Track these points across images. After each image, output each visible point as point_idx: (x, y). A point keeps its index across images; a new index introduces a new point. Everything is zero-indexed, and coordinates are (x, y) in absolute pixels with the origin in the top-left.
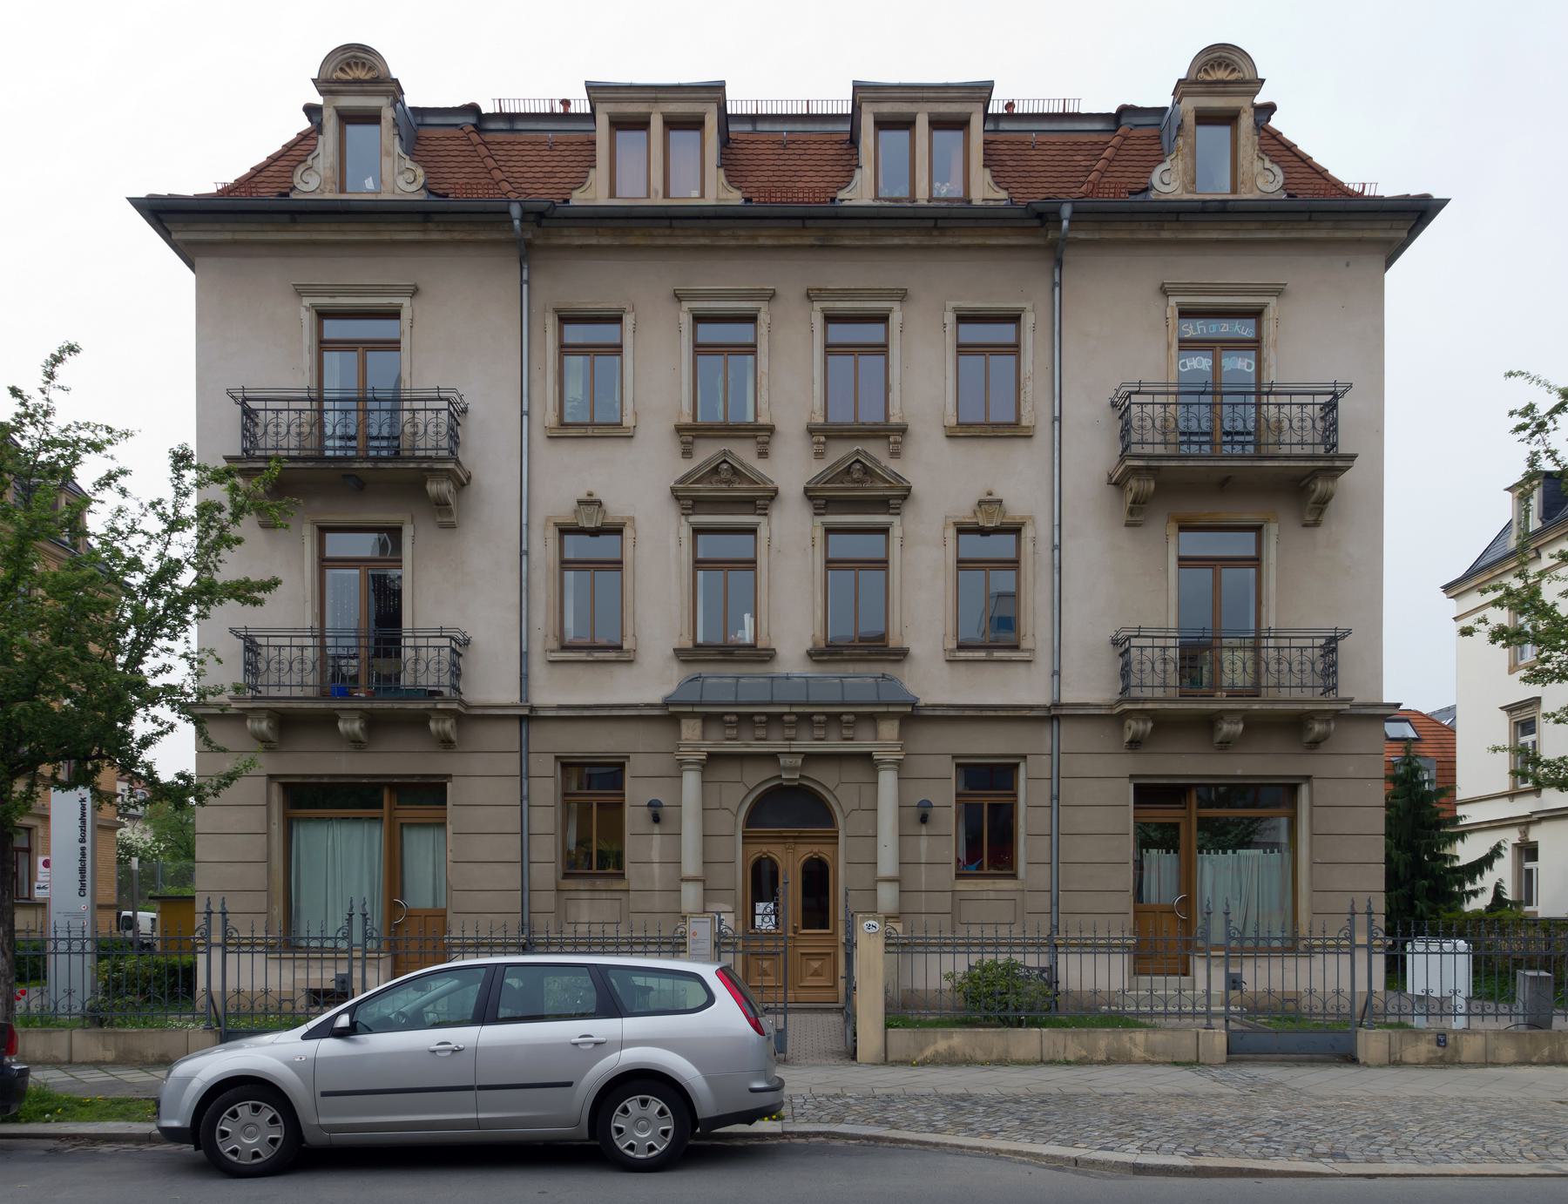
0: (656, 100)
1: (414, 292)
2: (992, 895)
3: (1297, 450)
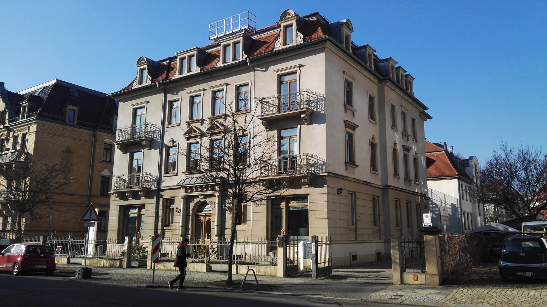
2: (241, 229)
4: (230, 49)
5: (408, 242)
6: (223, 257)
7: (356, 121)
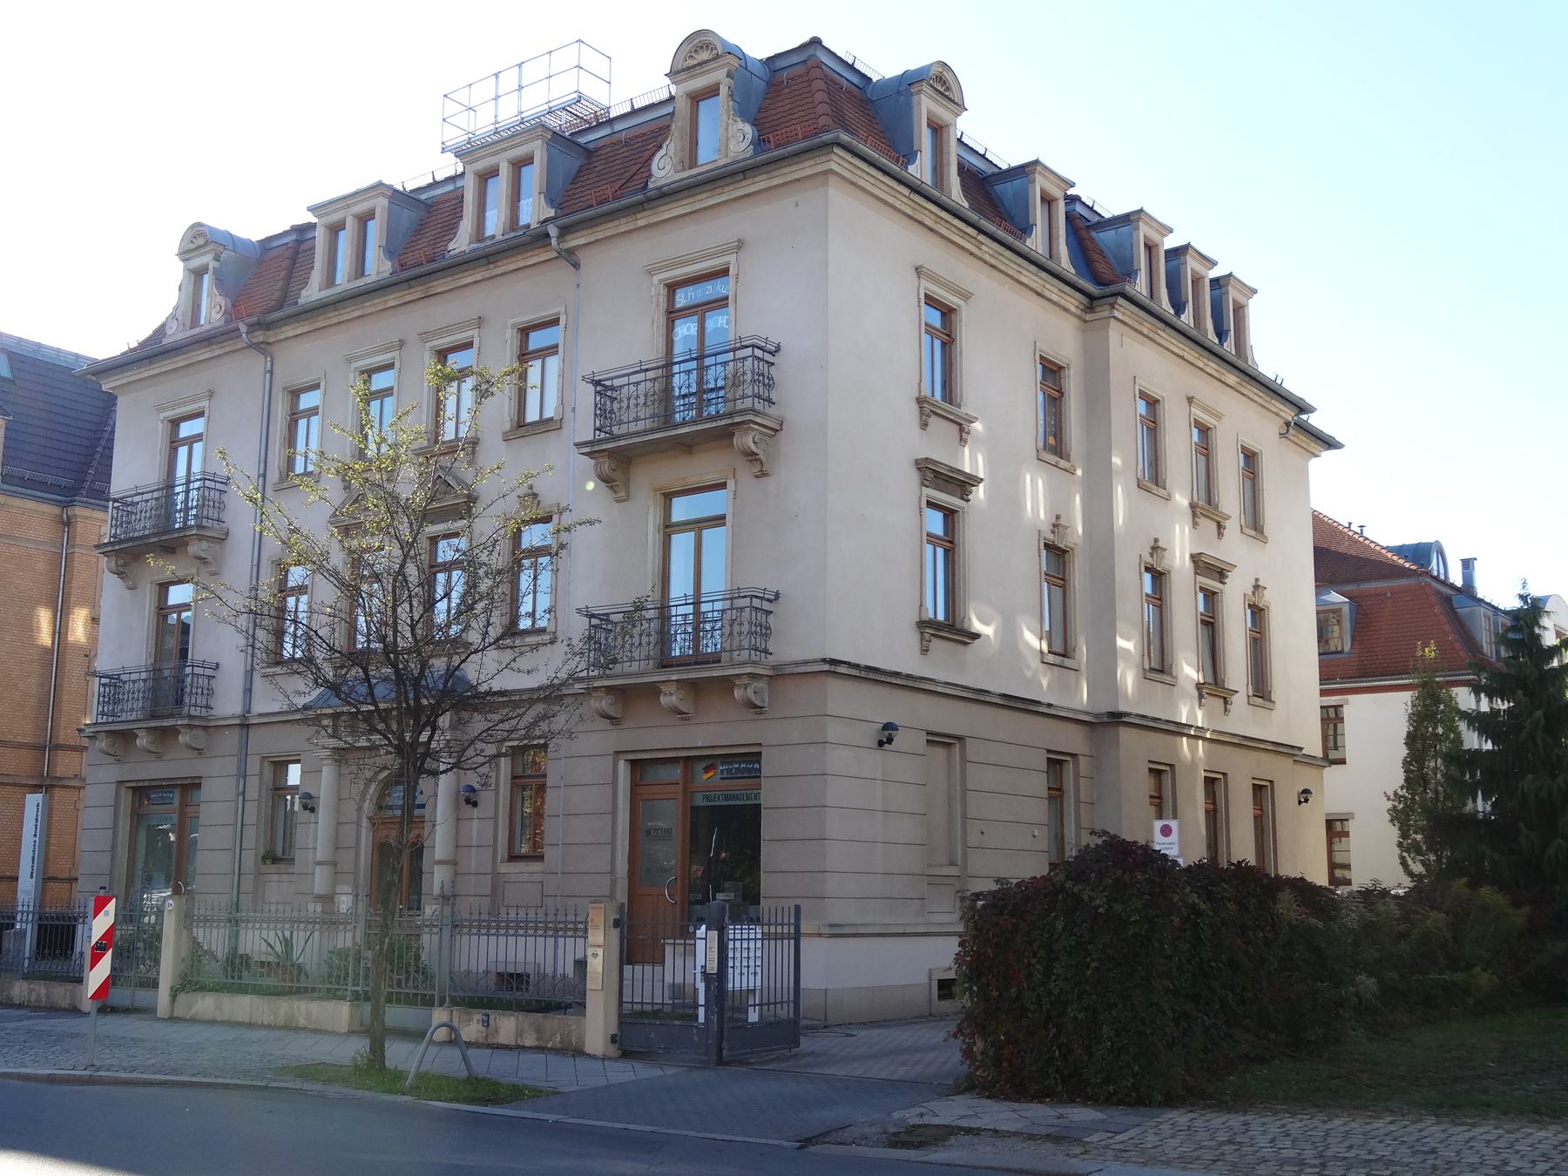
0: (348, 206)
2: (526, 877)
3: (633, 428)
5: (782, 925)
6: (407, 979)
7: (971, 461)
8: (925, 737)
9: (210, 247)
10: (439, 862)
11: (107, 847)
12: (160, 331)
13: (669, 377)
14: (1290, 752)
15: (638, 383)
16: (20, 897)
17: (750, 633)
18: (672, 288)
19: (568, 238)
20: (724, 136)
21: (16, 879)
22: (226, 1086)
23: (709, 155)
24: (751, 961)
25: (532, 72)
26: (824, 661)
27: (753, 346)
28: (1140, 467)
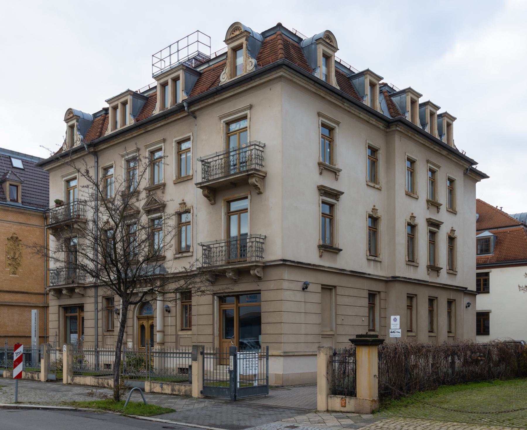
0: (119, 99)
1: (164, 141)
2: (187, 336)
3: (215, 177)
4: (169, 89)
8: (320, 286)
9: (75, 117)
10: (158, 332)
11: (57, 327)
12: (61, 149)
13: (228, 157)
14: (464, 291)
15: (216, 161)
16: (33, 343)
17: (256, 251)
18: (228, 124)
19: (192, 107)
20: (245, 64)
21: (30, 337)
22: (38, 408)
23: (240, 74)
24: (248, 365)
25: (182, 44)
26: (281, 260)
27: (255, 145)
28: (407, 186)
